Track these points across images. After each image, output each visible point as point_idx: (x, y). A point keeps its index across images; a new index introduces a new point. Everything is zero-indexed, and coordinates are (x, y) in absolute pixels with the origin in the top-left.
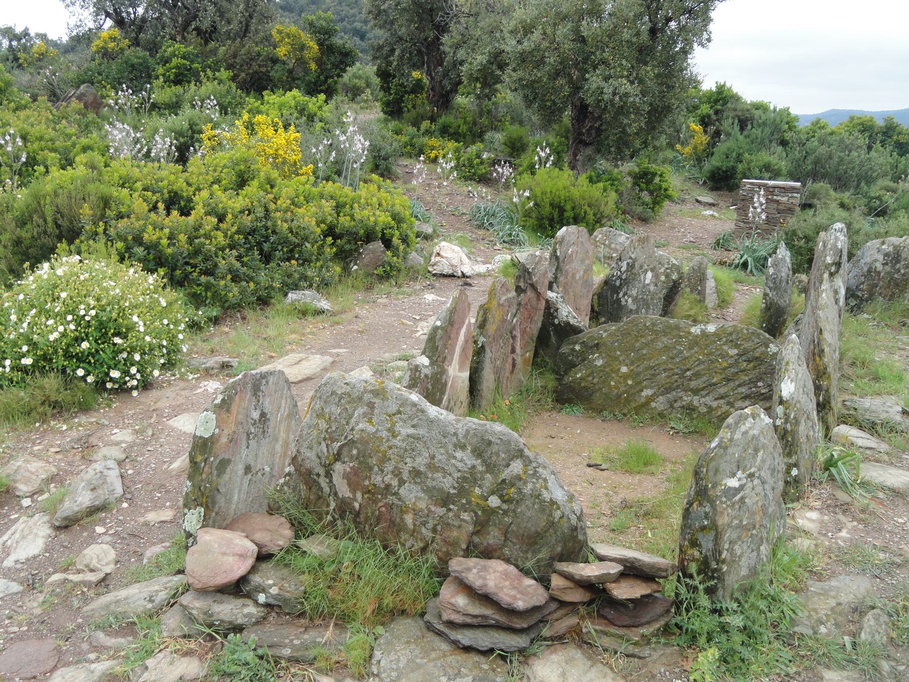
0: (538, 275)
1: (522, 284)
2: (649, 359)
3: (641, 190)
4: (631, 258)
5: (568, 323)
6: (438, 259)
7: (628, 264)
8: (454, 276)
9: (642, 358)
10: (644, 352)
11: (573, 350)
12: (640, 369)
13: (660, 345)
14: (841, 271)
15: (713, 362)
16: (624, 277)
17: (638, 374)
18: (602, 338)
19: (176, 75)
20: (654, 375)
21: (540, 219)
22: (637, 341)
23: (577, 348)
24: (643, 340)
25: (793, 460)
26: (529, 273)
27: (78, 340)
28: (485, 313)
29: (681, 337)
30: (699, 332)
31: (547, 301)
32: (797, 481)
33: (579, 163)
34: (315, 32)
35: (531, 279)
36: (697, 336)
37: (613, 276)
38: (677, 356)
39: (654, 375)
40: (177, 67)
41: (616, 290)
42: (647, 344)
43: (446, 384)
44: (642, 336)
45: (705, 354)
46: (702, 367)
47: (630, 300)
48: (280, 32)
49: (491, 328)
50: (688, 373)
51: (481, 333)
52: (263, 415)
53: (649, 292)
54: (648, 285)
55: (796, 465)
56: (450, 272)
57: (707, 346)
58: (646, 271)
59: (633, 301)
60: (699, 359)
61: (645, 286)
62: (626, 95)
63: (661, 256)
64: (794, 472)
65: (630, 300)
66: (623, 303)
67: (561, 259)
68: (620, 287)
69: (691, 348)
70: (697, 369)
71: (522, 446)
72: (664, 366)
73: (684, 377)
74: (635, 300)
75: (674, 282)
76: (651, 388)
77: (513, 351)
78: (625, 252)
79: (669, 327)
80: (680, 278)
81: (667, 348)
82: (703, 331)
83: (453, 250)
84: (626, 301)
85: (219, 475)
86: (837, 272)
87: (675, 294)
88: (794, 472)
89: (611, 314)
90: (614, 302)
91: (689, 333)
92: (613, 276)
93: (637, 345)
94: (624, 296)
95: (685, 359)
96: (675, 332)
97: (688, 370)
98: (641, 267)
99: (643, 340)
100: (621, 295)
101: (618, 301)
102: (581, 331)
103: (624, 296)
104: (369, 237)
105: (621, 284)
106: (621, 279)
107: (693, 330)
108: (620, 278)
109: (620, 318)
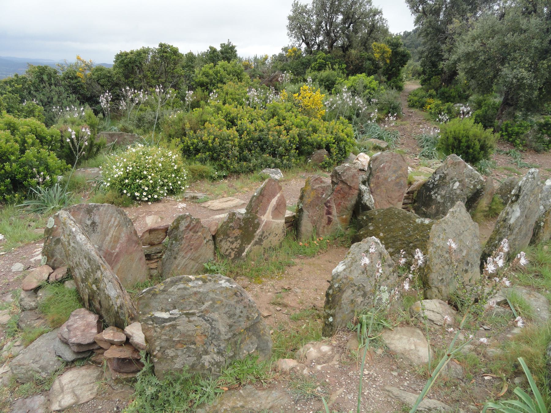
0: (347, 176)
1: (335, 180)
2: (393, 232)
3: (543, 134)
4: (443, 173)
5: (366, 204)
6: (357, 161)
7: (440, 176)
8: (363, 170)
9: (390, 231)
10: (392, 227)
11: (363, 219)
12: (389, 236)
13: (399, 225)
14: (519, 201)
15: (424, 241)
16: (436, 183)
17: (388, 239)
18: (375, 215)
19: (319, 67)
20: (395, 241)
21: (448, 145)
22: (390, 221)
23: (365, 218)
24: (392, 221)
25: (332, 312)
26: (339, 175)
27: (125, 178)
28: (303, 193)
29: (410, 223)
30: (420, 222)
31: (360, 190)
32: (331, 325)
33: (504, 116)
34: (390, 45)
35: (341, 178)
36: (418, 224)
37: (429, 182)
38: (407, 233)
39: (395, 241)
40: (319, 63)
41: (430, 190)
42: (394, 223)
43: (258, 224)
44: (393, 219)
45: (420, 236)
46: (418, 243)
47: (439, 197)
48: (375, 46)
49: (307, 200)
50: (411, 244)
51: (301, 202)
52: (93, 223)
53: (456, 194)
54: (455, 189)
55: (333, 316)
56: (362, 168)
57: (422, 231)
58: (455, 181)
59: (441, 197)
60: (417, 238)
61: (452, 190)
62: (523, 78)
63: (476, 174)
64: (331, 319)
65: (439, 197)
66: (434, 197)
67: (373, 169)
68: (433, 189)
69: (414, 231)
70: (416, 243)
71: (100, 264)
72: (400, 238)
73: (409, 246)
74: (443, 197)
75: (478, 190)
76: (392, 248)
77: (329, 213)
78: (440, 169)
79: (405, 216)
80: (482, 188)
81: (403, 228)
82: (422, 222)
83: (364, 158)
84: (436, 197)
85: (55, 245)
86: (516, 200)
87: (478, 197)
88: (331, 319)
89: (424, 203)
90: (427, 196)
91: (415, 222)
92: (429, 182)
93: (390, 222)
94: (435, 194)
95: (410, 236)
96: (408, 220)
97: (411, 243)
98: (452, 179)
99: (392, 221)
100: (432, 193)
101: (430, 196)
102: (370, 209)
103: (435, 194)
104: (319, 147)
105: (433, 187)
106: (434, 184)
107: (417, 220)
108: (433, 183)
109: (431, 206)
